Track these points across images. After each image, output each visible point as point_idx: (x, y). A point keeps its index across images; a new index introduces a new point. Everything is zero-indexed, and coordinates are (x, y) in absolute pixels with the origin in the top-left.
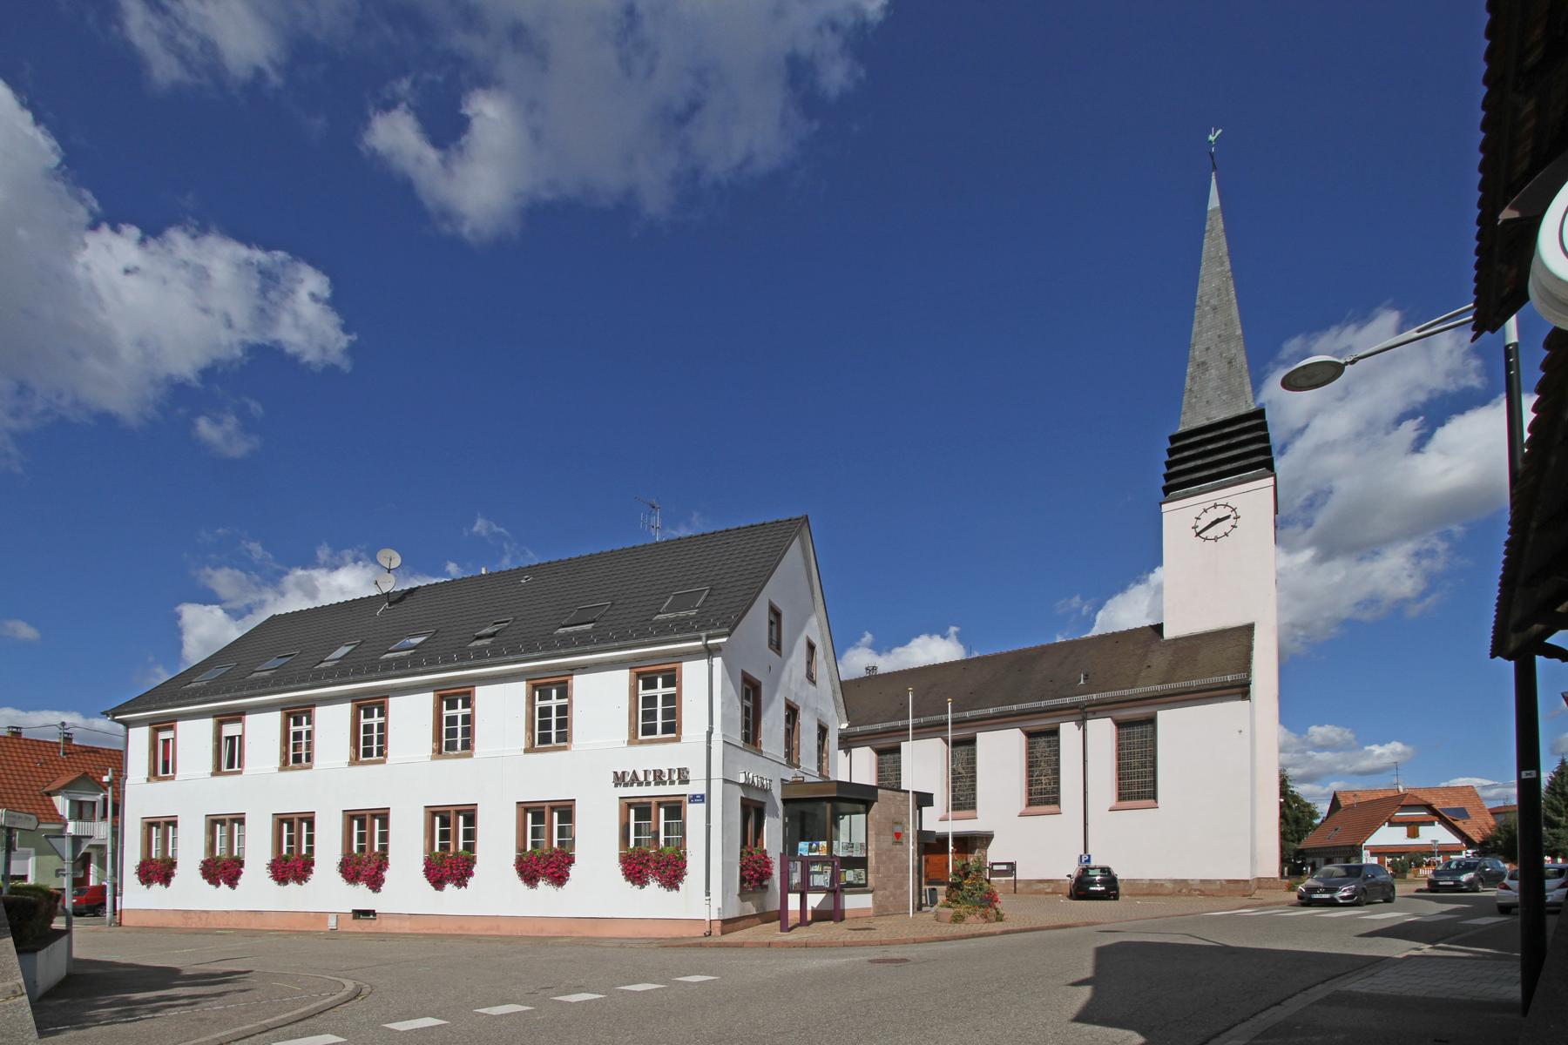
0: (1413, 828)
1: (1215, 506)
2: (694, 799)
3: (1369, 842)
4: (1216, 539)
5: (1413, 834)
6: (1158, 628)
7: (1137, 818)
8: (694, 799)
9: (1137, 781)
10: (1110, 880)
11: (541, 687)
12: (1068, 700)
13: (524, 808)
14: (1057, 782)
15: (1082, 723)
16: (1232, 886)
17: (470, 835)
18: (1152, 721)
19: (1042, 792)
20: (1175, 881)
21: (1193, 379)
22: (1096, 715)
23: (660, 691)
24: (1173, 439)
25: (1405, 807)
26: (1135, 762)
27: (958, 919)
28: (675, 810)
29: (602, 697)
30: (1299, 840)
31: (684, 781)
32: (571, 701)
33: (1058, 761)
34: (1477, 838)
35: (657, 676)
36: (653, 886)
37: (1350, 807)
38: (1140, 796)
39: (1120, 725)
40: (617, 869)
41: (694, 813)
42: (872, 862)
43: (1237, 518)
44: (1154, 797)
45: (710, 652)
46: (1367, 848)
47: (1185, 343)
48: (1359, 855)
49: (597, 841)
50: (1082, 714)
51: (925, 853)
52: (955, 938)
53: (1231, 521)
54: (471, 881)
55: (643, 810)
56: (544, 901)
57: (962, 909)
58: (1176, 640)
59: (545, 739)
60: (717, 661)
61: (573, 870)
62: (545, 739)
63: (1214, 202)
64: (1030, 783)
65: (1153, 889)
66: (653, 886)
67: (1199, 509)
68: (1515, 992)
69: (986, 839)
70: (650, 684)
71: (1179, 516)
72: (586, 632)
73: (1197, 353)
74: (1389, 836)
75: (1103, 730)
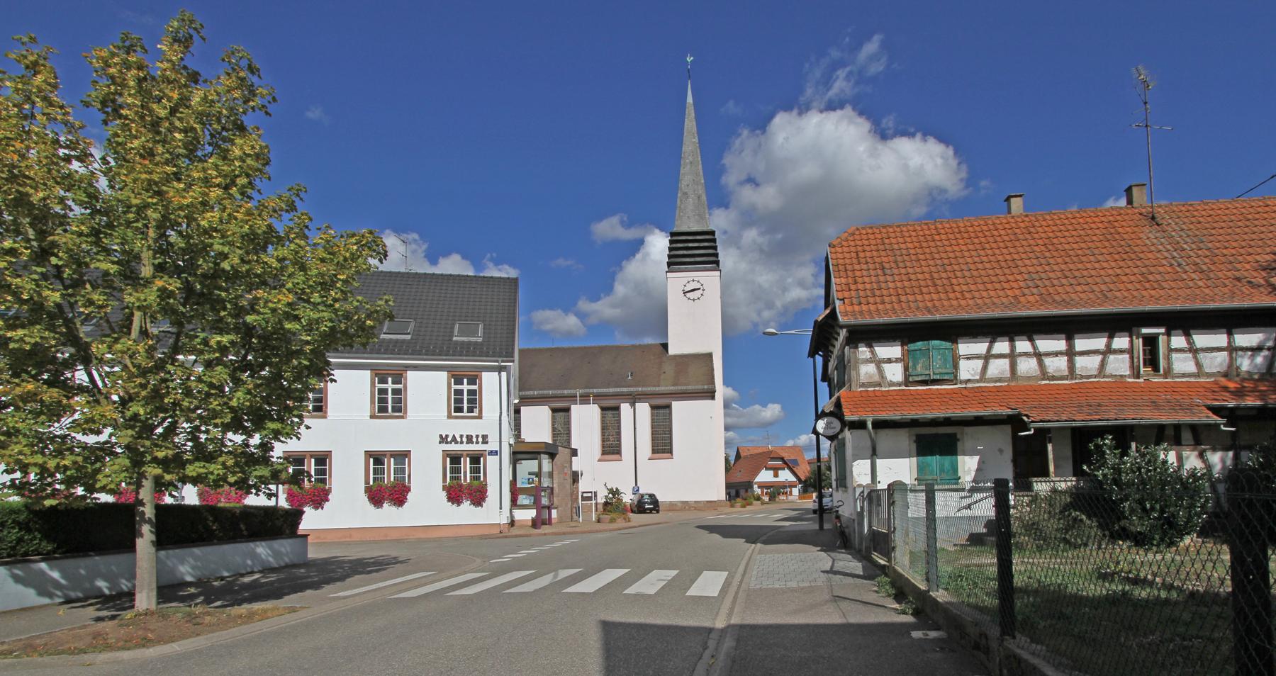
0: (776, 470)
2: (492, 453)
3: (758, 479)
5: (776, 475)
6: (665, 346)
7: (662, 464)
8: (492, 453)
9: (662, 445)
10: (655, 502)
11: (380, 375)
12: (625, 390)
13: (369, 454)
14: (619, 440)
15: (633, 405)
17: (322, 472)
18: (669, 407)
19: (611, 448)
23: (465, 387)
25: (773, 459)
26: (661, 430)
27: (613, 521)
28: (476, 459)
29: (427, 388)
31: (485, 442)
32: (405, 387)
33: (619, 427)
34: (803, 478)
35: (610, 412)
36: (466, 504)
37: (746, 457)
38: (664, 452)
39: (653, 407)
41: (492, 462)
42: (556, 490)
44: (671, 452)
45: (500, 369)
47: (677, 180)
48: (752, 487)
49: (427, 478)
50: (633, 399)
52: (597, 531)
53: (700, 292)
54: (327, 505)
55: (455, 459)
56: (388, 516)
57: (613, 515)
58: (675, 357)
59: (383, 409)
60: (504, 374)
61: (409, 496)
62: (383, 409)
63: (690, 99)
64: (603, 440)
65: (672, 506)
66: (466, 504)
68: (816, 527)
70: (459, 381)
72: (404, 341)
73: (683, 184)
74: (765, 476)
75: (644, 409)
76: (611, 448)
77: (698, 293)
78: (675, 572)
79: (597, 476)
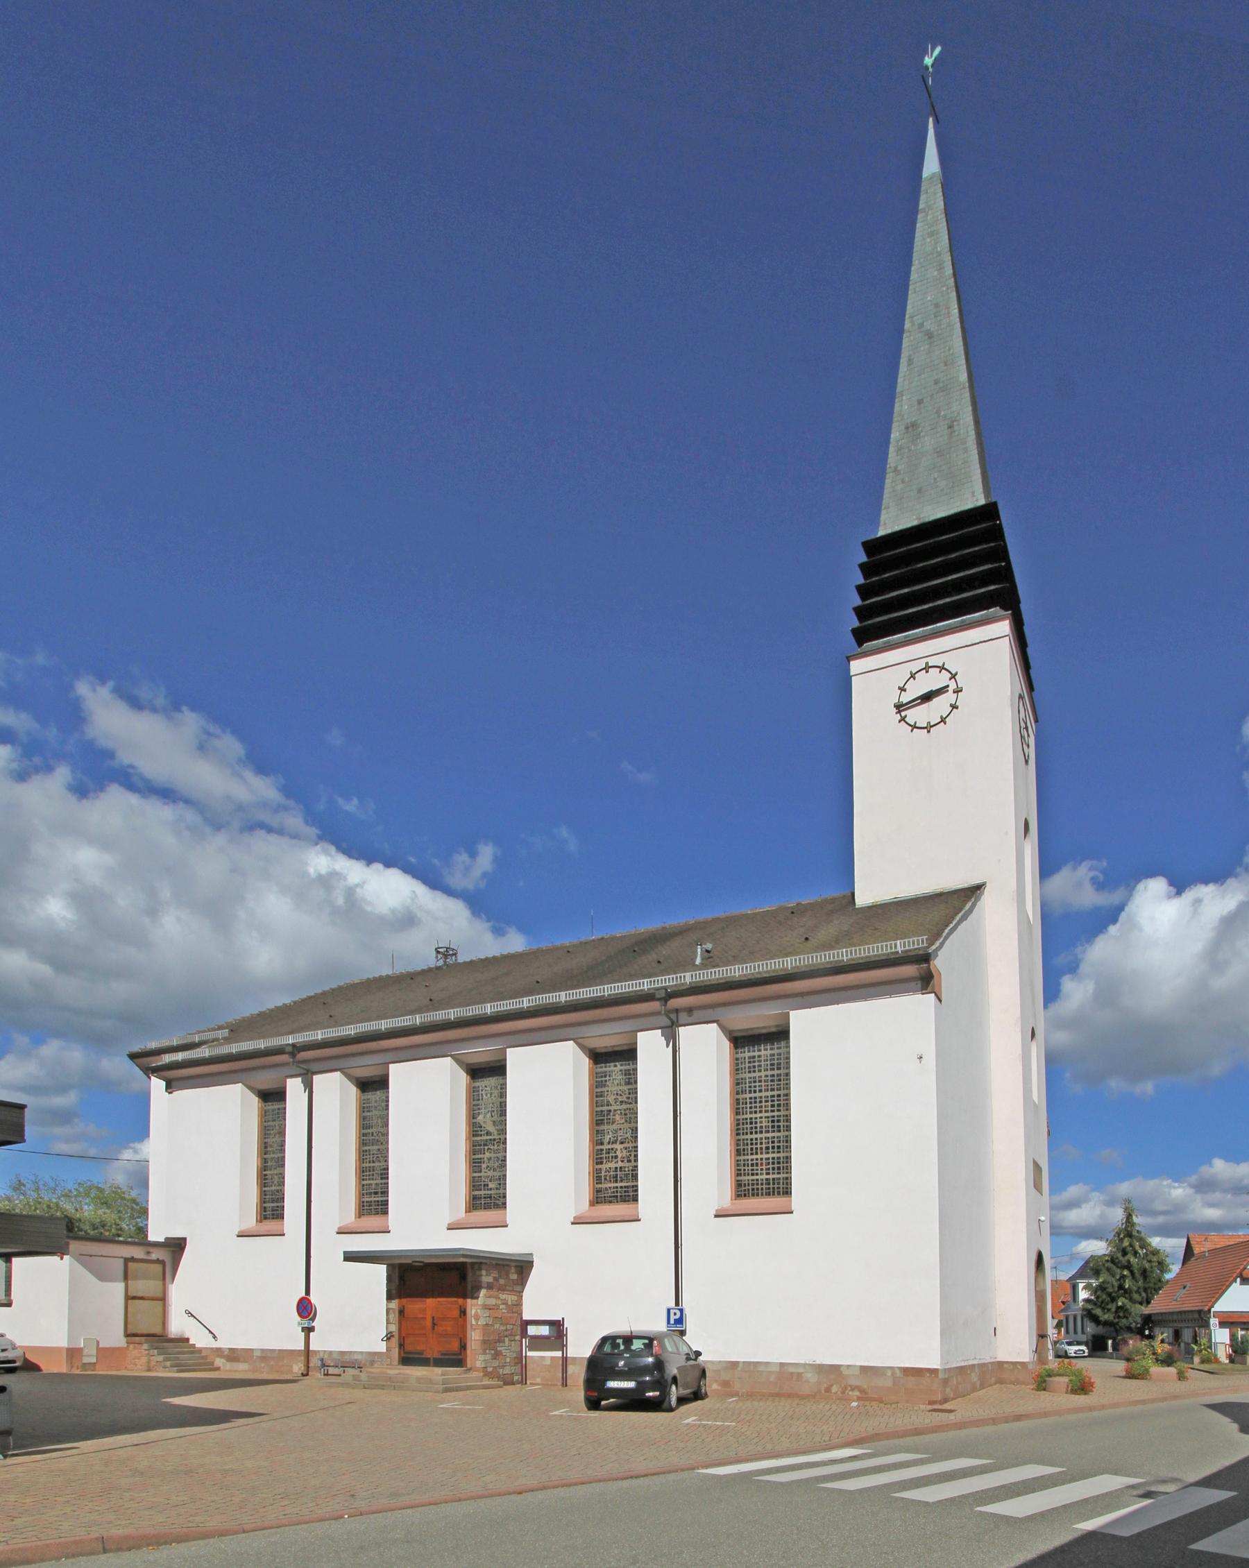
1: (927, 668)
3: (1218, 1307)
4: (929, 728)
7: (758, 1231)
9: (762, 1172)
15: (671, 1037)
16: (911, 1382)
19: (613, 1186)
20: (821, 1369)
21: (899, 449)
22: (694, 1016)
24: (872, 547)
30: (1148, 1302)
40: (72, 799)
43: (953, 676)
46: (1217, 1314)
48: (1206, 1325)
51: (399, 1296)
53: (949, 697)
63: (932, 165)
65: (782, 1387)
67: (904, 672)
69: (521, 1267)
71: (878, 677)
75: (705, 1046)
76: (613, 1186)
77: (940, 705)
78: (1194, 1547)
79: (588, 1285)
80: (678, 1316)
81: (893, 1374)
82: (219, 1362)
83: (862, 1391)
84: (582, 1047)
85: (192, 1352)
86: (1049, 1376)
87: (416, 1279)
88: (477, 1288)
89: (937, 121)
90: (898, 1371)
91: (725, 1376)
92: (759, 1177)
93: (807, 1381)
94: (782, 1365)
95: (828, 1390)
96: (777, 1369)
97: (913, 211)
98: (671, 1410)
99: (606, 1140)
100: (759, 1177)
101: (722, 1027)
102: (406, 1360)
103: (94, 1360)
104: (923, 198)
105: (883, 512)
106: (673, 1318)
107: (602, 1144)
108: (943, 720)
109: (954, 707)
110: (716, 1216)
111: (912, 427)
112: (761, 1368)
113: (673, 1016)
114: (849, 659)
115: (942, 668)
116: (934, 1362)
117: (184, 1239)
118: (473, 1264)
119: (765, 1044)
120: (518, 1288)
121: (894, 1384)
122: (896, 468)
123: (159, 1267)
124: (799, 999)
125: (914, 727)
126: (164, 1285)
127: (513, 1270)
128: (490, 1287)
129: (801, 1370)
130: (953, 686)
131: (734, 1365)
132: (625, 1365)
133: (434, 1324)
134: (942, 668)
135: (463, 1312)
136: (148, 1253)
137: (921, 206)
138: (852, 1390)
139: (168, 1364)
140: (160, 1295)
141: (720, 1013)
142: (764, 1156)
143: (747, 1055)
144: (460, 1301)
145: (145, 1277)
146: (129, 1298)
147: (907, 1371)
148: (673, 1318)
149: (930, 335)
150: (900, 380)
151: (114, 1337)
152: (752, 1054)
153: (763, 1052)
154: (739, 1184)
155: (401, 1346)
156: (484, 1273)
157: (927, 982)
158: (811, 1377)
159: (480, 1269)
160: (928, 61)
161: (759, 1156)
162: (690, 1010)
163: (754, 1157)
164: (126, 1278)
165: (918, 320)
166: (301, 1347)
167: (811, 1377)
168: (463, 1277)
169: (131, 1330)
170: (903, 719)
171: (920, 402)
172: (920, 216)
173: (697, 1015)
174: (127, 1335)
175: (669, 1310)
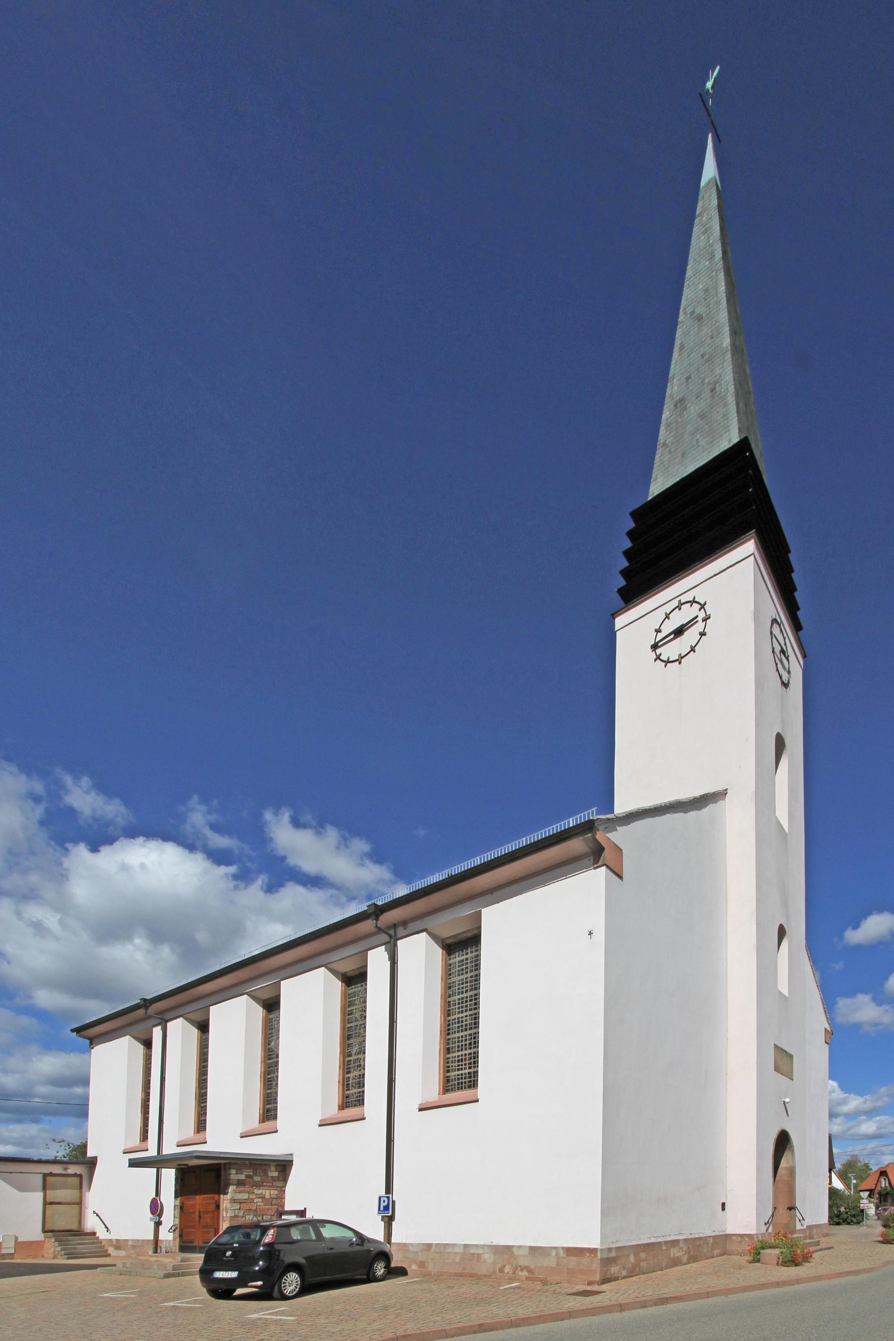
1: (679, 607)
43: (702, 607)
51: (181, 1196)
53: (699, 626)
63: (710, 170)
69: (284, 1166)
77: (691, 636)
80: (386, 1204)
81: (557, 1255)
82: (111, 1250)
83: (530, 1271)
84: (334, 972)
85: (97, 1243)
86: (763, 1248)
87: (202, 1178)
88: (227, 1185)
89: (718, 140)
90: (561, 1251)
91: (422, 1257)
92: (463, 1072)
93: (485, 1261)
94: (466, 1246)
95: (501, 1270)
96: (461, 1250)
97: (691, 216)
98: (285, 1298)
99: (354, 1052)
100: (463, 1072)
101: (431, 934)
102: (183, 1248)
103: (12, 1251)
104: (700, 204)
105: (652, 485)
106: (383, 1205)
107: (350, 1056)
108: (693, 649)
109: (703, 634)
110: (420, 1110)
111: (681, 403)
112: (449, 1250)
113: (392, 932)
114: (614, 615)
115: (693, 601)
116: (593, 1241)
117: (96, 1158)
118: (225, 1164)
119: (471, 947)
120: (279, 1184)
121: (558, 1265)
122: (664, 443)
123: (76, 1180)
124: (489, 897)
125: (668, 662)
126: (81, 1193)
127: (273, 1168)
128: (240, 1183)
129: (480, 1251)
130: (702, 615)
131: (429, 1246)
132: (231, 1256)
133: (200, 1217)
134: (693, 601)
135: (218, 1207)
136: (66, 1169)
137: (698, 212)
138: (522, 1270)
139: (63, 1253)
140: (78, 1201)
141: (429, 922)
142: (468, 1051)
143: (458, 959)
144: (216, 1196)
145: (64, 1187)
146: (46, 1203)
147: (570, 1251)
148: (383, 1205)
149: (699, 318)
150: (672, 366)
151: (33, 1231)
152: (461, 958)
153: (470, 955)
154: (447, 1080)
155: (181, 1236)
156: (233, 1171)
157: (596, 855)
158: (488, 1257)
159: (230, 1169)
160: (709, 85)
161: (464, 1052)
162: (404, 923)
163: (460, 1053)
164: (44, 1188)
165: (689, 310)
166: (151, 1237)
167: (488, 1257)
168: (219, 1176)
169: (46, 1229)
170: (658, 658)
171: (688, 379)
172: (697, 221)
173: (412, 926)
174: (44, 1231)
175: (380, 1198)
